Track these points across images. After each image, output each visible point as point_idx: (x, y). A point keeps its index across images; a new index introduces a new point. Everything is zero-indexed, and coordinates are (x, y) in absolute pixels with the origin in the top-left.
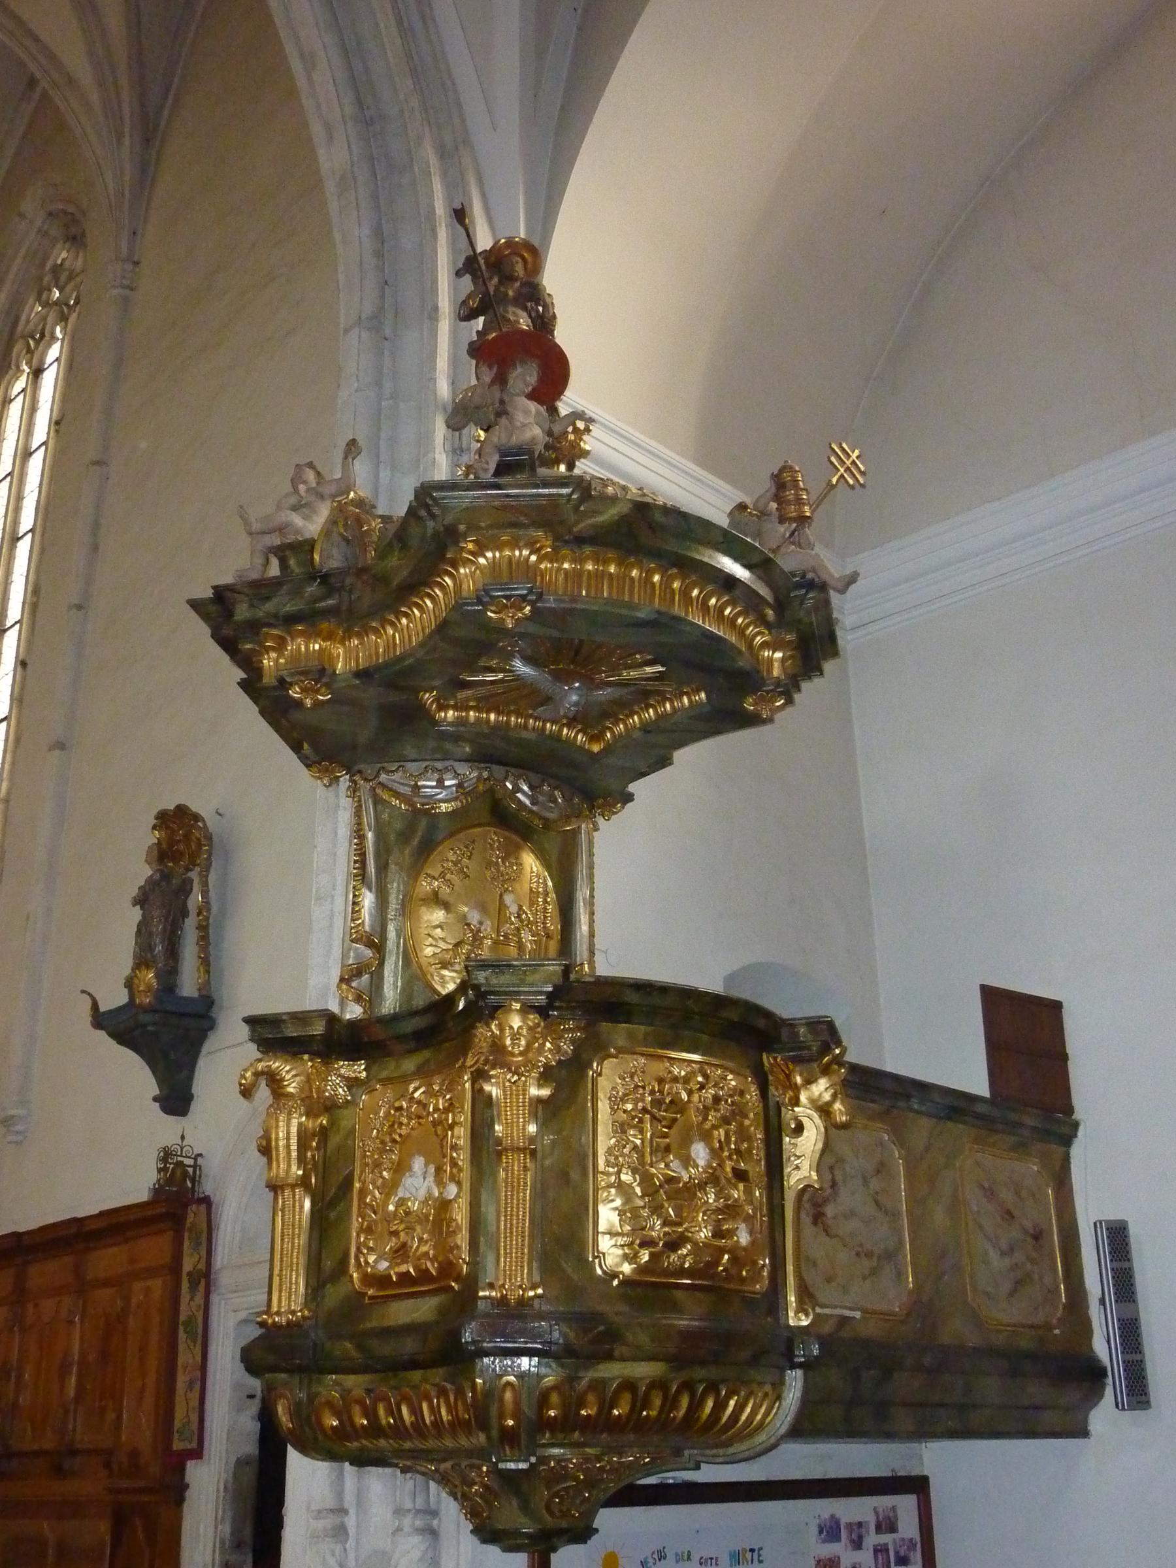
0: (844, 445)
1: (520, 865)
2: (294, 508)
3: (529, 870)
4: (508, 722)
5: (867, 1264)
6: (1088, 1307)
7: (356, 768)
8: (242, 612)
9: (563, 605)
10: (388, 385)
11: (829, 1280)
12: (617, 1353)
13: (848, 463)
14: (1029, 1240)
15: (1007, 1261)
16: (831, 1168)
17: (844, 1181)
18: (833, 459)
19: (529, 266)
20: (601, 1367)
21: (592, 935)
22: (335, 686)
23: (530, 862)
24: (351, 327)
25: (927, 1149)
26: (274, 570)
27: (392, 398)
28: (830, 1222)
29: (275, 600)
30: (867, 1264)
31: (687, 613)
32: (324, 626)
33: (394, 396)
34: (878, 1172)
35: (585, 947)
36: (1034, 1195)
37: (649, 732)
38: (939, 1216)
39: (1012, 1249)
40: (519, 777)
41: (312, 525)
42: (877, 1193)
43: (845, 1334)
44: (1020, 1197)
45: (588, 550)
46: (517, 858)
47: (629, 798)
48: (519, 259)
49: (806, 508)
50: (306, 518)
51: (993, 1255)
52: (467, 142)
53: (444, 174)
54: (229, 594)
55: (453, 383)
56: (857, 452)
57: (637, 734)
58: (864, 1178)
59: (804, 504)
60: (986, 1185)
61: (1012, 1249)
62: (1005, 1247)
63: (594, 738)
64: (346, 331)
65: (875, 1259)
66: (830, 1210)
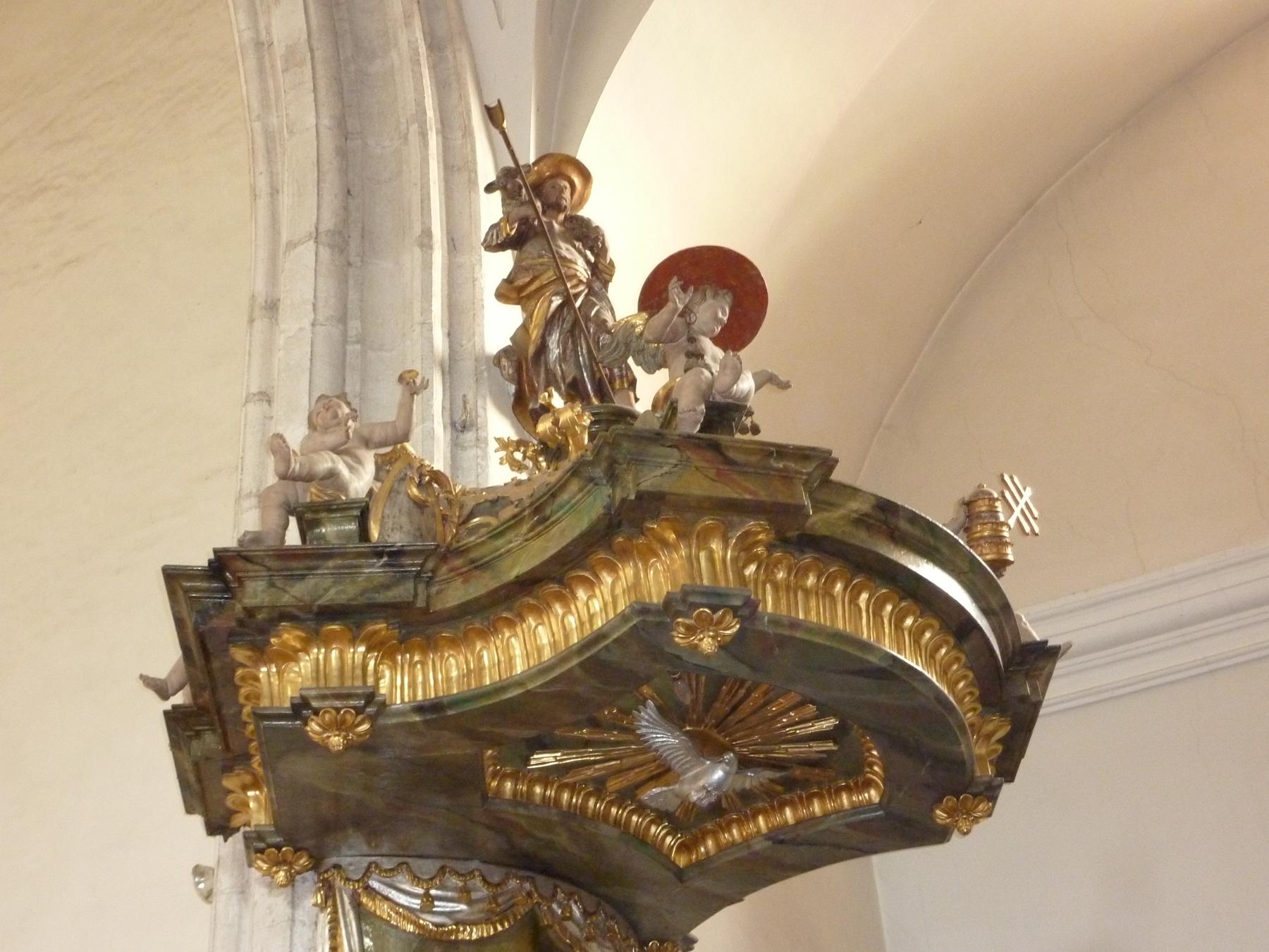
2: (337, 450)
4: (584, 807)
8: (256, 592)
9: (779, 631)
10: (354, 326)
22: (381, 721)
24: (300, 242)
26: (293, 537)
27: (358, 342)
29: (311, 582)
33: (361, 340)
37: (782, 842)
40: (570, 896)
41: (360, 480)
45: (808, 559)
47: (693, 941)
49: (1009, 550)
50: (351, 468)
52: (465, 34)
53: (434, 67)
54: (240, 564)
55: (449, 335)
57: (759, 845)
59: (1006, 544)
63: (684, 848)
64: (292, 245)
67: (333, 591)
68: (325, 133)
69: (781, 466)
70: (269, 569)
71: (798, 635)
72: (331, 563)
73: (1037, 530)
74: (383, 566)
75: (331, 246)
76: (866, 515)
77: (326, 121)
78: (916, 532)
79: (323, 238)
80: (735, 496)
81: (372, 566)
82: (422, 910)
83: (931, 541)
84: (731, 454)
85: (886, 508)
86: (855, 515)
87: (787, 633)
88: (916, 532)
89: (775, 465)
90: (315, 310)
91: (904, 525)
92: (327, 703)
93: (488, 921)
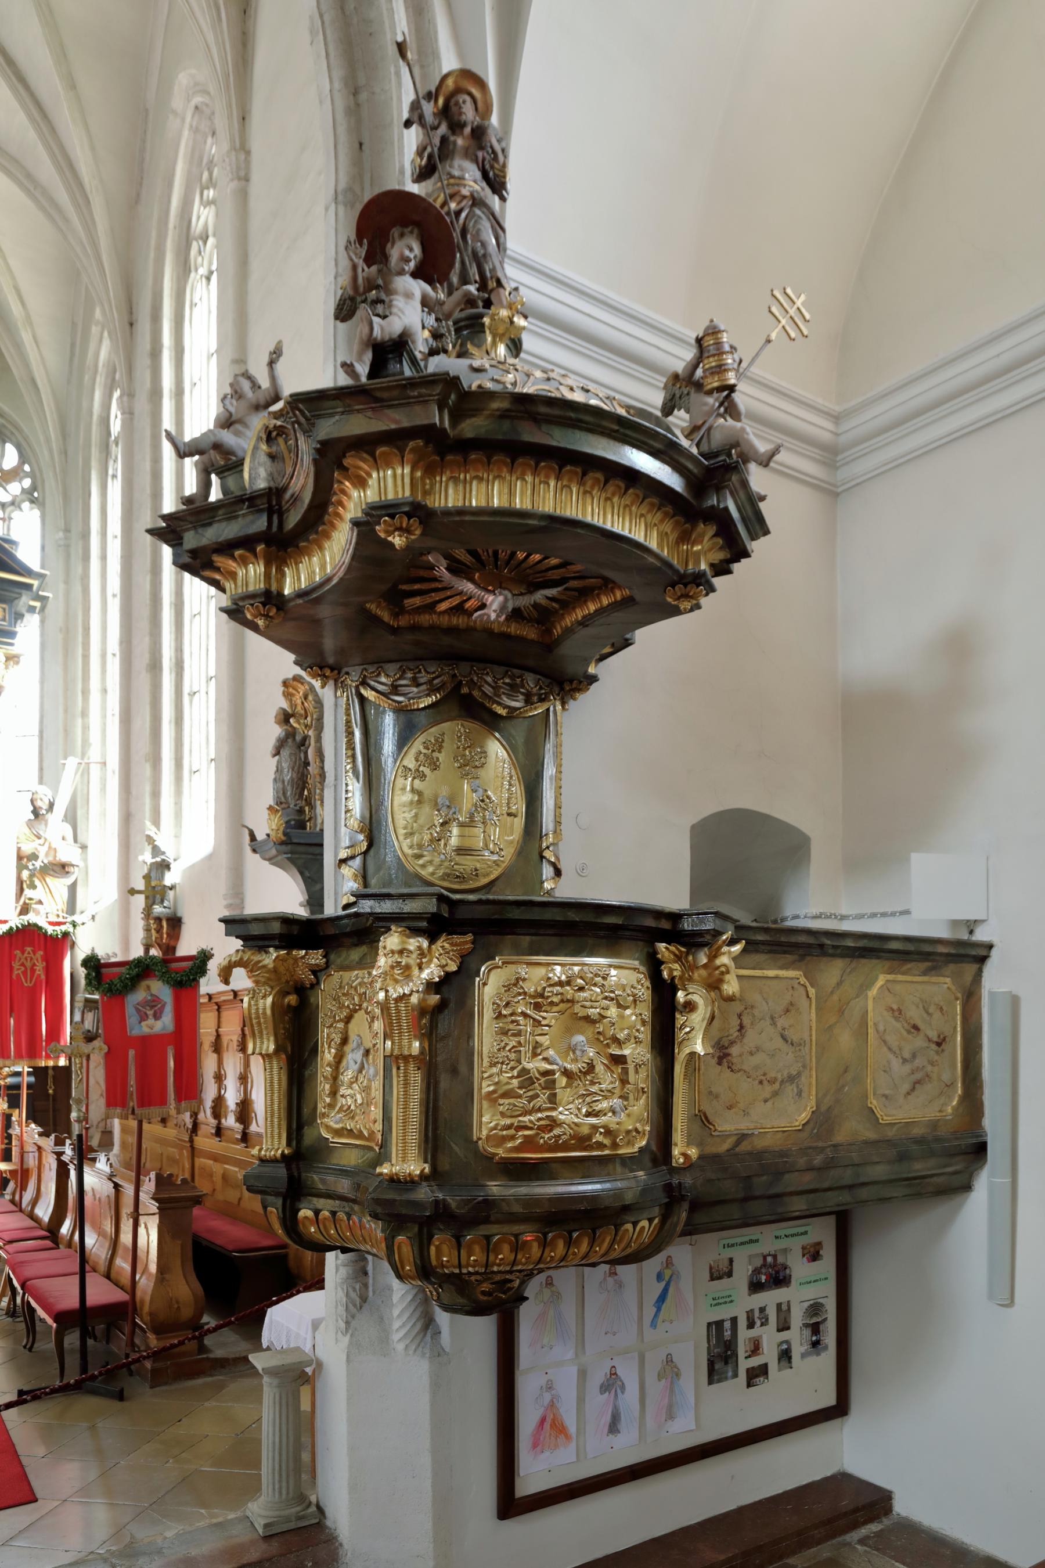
0: (789, 291)
1: (484, 753)
3: (494, 756)
5: (768, 1089)
6: (982, 1094)
7: (345, 670)
11: (730, 1108)
12: (492, 1218)
13: (792, 312)
14: (934, 1047)
15: (907, 1068)
16: (740, 1016)
17: (752, 1024)
18: (774, 309)
19: (480, 104)
20: (481, 1227)
21: (558, 806)
23: (496, 750)
25: (839, 984)
28: (735, 1060)
30: (768, 1089)
31: (584, 513)
32: (237, 553)
34: (788, 1011)
35: (551, 818)
36: (941, 1009)
38: (845, 1039)
39: (914, 1056)
42: (784, 1029)
43: (745, 1147)
44: (927, 1012)
46: (481, 747)
48: (468, 98)
50: (237, 434)
51: (896, 1063)
56: (803, 297)
58: (772, 1018)
60: (895, 1007)
61: (914, 1056)
62: (907, 1055)
65: (777, 1084)
66: (734, 1051)
67: (226, 531)
68: (338, 97)
69: (416, 394)
70: (191, 523)
71: (467, 518)
72: (220, 512)
73: (806, 333)
74: (248, 508)
75: (345, 205)
76: (507, 410)
77: (337, 85)
78: (557, 412)
79: (340, 198)
80: (384, 428)
81: (242, 509)
82: (391, 693)
83: (573, 415)
84: (378, 394)
85: (523, 400)
86: (498, 413)
87: (457, 519)
88: (557, 412)
89: (412, 394)
90: (336, 265)
91: (543, 409)
92: (247, 602)
93: (428, 695)
